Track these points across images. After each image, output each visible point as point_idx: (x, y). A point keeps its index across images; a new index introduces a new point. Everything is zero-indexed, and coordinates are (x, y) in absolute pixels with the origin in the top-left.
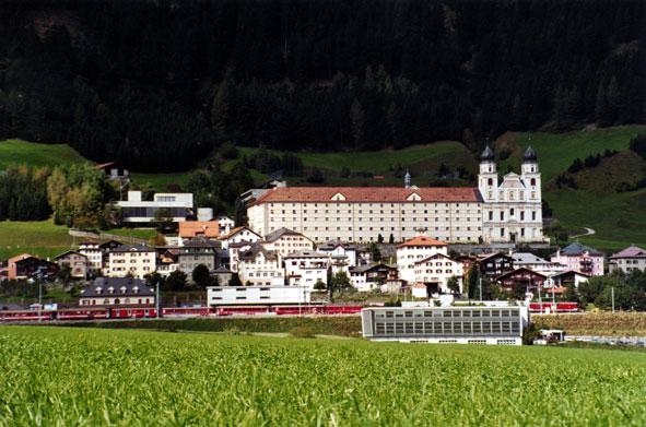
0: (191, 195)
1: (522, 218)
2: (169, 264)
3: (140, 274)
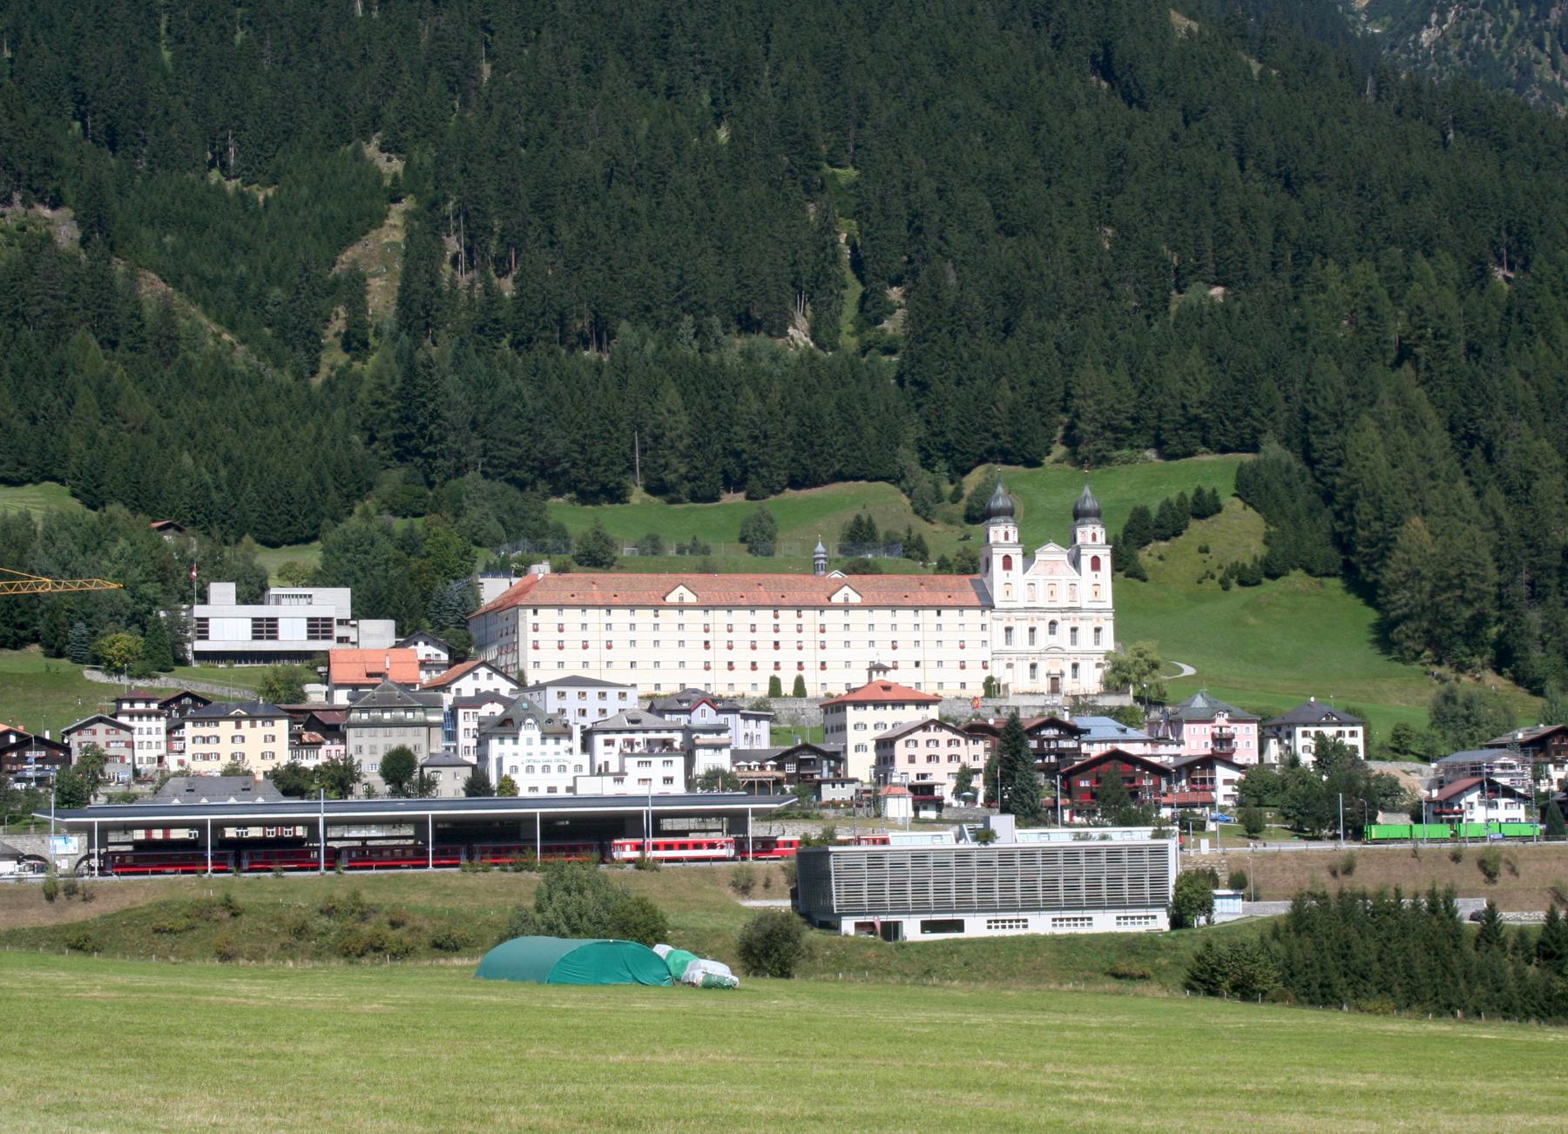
0: (347, 591)
1: (1074, 642)
2: (319, 744)
3: (259, 767)
